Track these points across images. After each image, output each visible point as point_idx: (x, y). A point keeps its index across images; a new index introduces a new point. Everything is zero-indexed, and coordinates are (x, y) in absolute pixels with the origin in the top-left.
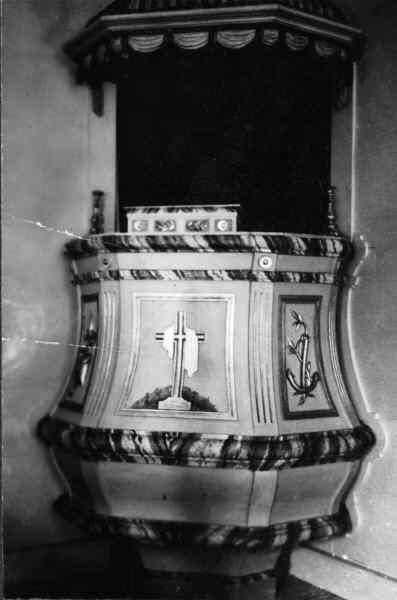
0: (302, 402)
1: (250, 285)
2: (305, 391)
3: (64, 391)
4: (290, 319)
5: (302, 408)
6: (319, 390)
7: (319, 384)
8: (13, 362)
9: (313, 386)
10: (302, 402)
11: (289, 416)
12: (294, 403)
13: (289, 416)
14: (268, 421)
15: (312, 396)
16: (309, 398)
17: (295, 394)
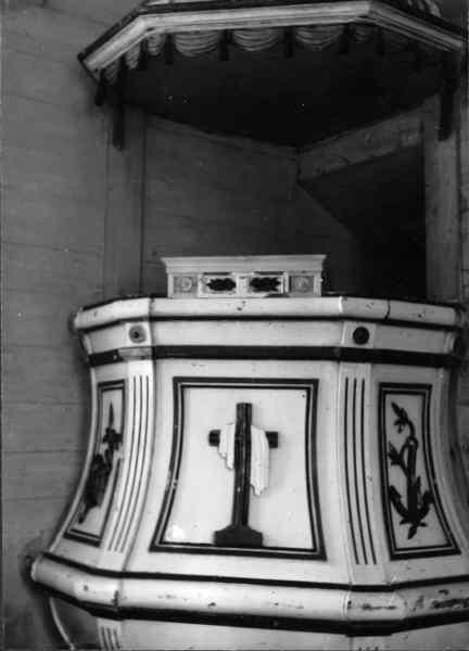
0: (412, 533)
1: (155, 365)
2: (414, 518)
3: (286, 24)
4: (391, 417)
5: (413, 543)
6: (431, 518)
7: (431, 506)
8: (95, 624)
9: (425, 511)
10: (412, 533)
11: (396, 554)
12: (402, 540)
13: (396, 554)
14: (119, 549)
15: (423, 525)
16: (419, 528)
17: (402, 523)
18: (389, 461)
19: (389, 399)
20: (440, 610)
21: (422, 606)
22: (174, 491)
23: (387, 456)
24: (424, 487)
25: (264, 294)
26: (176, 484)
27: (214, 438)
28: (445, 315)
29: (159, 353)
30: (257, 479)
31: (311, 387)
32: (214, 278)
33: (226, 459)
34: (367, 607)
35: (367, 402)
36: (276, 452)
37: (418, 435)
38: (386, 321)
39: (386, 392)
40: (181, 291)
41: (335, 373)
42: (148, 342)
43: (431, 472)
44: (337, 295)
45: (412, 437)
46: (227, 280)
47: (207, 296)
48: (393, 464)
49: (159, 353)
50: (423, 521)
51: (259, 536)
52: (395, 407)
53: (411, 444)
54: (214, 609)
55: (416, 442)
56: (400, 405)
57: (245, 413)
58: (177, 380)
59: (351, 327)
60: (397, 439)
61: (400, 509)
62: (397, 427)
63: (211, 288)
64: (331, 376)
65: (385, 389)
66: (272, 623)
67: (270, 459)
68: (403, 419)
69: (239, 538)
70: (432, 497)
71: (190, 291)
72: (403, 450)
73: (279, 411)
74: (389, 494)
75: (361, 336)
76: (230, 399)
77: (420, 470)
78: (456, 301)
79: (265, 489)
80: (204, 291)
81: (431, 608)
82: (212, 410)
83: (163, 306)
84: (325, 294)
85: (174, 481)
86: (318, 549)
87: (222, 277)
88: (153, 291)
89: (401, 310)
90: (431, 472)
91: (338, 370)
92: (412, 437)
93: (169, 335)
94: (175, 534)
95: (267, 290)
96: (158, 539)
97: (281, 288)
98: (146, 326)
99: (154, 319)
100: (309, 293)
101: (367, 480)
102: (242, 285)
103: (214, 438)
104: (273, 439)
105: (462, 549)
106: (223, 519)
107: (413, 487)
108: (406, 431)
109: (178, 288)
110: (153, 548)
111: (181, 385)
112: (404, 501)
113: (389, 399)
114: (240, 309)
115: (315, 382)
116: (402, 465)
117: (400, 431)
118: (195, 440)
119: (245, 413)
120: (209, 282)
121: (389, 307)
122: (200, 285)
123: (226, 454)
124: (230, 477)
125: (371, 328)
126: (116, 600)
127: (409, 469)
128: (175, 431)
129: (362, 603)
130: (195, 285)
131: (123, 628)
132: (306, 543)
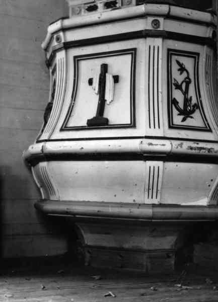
0: (184, 120)
1: (66, 52)
2: (186, 113)
4: (175, 67)
6: (197, 114)
9: (193, 112)
10: (184, 120)
11: (172, 126)
13: (172, 126)
15: (192, 117)
18: (174, 87)
19: (174, 58)
20: (193, 152)
21: (181, 147)
22: (73, 106)
23: (171, 84)
24: (194, 101)
25: (110, 9)
26: (74, 104)
27: (90, 82)
28: (206, 16)
29: (68, 46)
30: (108, 97)
31: (133, 52)
32: (89, 5)
33: (95, 89)
34: (150, 144)
35: (160, 61)
36: (118, 85)
37: (192, 77)
38: (168, 16)
39: (172, 54)
40: (75, 14)
41: (145, 45)
42: (63, 41)
43: (198, 94)
44: (142, 4)
45: (188, 78)
46: (95, 5)
47: (86, 14)
48: (176, 89)
49: (68, 46)
50: (191, 115)
51: (107, 120)
52: (178, 62)
53: (188, 82)
54: (83, 151)
55: (190, 79)
56: (181, 62)
57: (105, 68)
58: (75, 57)
59: (150, 19)
60: (179, 78)
61: (178, 109)
62: (179, 72)
63: (88, 11)
64: (141, 45)
65: (171, 53)
66: (182, 254)
67: (114, 87)
68: (182, 69)
69: (99, 122)
70: (198, 106)
71: (78, 14)
72: (182, 82)
73: (120, 65)
74: (172, 102)
75: (156, 23)
76: (97, 64)
77: (192, 93)
78: (211, 9)
79: (112, 101)
80: (85, 12)
81: (188, 149)
82: (90, 69)
83: (67, 23)
84: (137, 4)
85: (73, 102)
86: (133, 124)
87: (92, 4)
88: (62, 16)
89: (177, 11)
90: (198, 94)
91: (146, 43)
92: (188, 78)
93: (72, 36)
94: (71, 124)
95: (112, 7)
96: (64, 126)
97: (118, 5)
98: (61, 34)
99: (64, 29)
100: (130, 5)
101: (159, 93)
102: (100, 6)
103: (90, 82)
104: (116, 79)
105: (213, 131)
106: (92, 113)
107: (187, 101)
108: (185, 74)
109: (74, 13)
110: (62, 130)
111: (77, 59)
112: (181, 105)
113: (174, 58)
114: (99, 18)
115: (135, 50)
116: (182, 91)
117: (181, 74)
118: (83, 84)
119: (105, 68)
120: (87, 8)
121: (170, 9)
122: (83, 10)
123: (95, 87)
124: (97, 97)
125: (161, 20)
126: (42, 150)
127: (185, 92)
128: (74, 80)
129: (148, 143)
130: (81, 10)
131: (48, 165)
132: (127, 121)
